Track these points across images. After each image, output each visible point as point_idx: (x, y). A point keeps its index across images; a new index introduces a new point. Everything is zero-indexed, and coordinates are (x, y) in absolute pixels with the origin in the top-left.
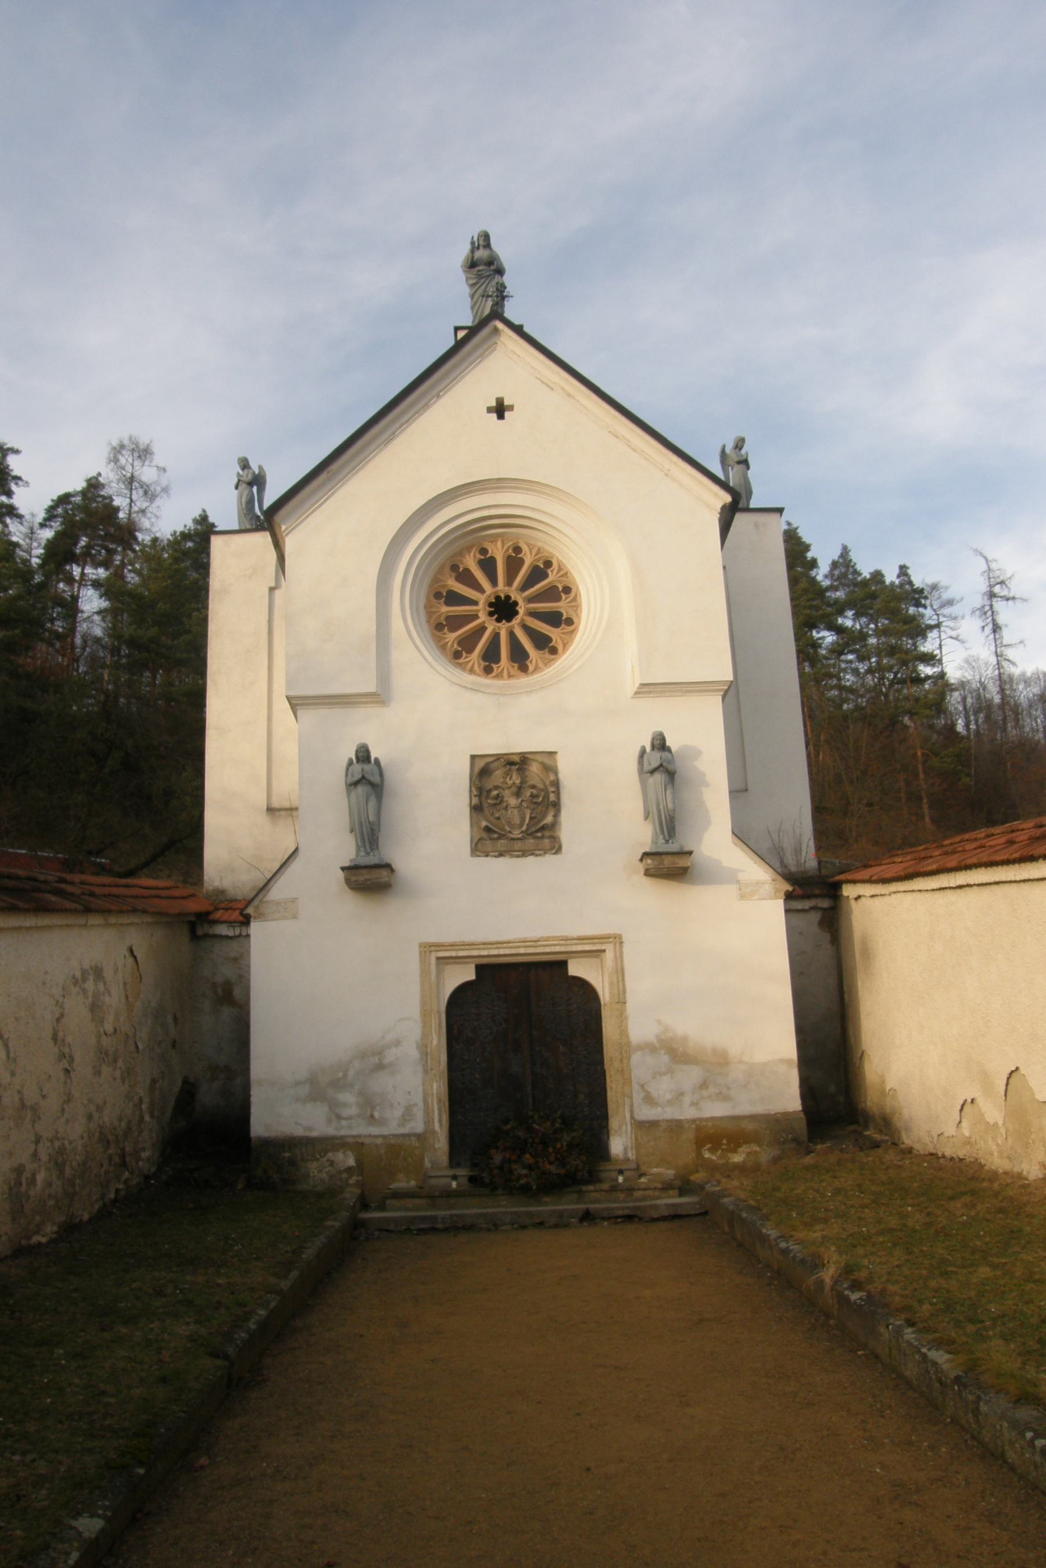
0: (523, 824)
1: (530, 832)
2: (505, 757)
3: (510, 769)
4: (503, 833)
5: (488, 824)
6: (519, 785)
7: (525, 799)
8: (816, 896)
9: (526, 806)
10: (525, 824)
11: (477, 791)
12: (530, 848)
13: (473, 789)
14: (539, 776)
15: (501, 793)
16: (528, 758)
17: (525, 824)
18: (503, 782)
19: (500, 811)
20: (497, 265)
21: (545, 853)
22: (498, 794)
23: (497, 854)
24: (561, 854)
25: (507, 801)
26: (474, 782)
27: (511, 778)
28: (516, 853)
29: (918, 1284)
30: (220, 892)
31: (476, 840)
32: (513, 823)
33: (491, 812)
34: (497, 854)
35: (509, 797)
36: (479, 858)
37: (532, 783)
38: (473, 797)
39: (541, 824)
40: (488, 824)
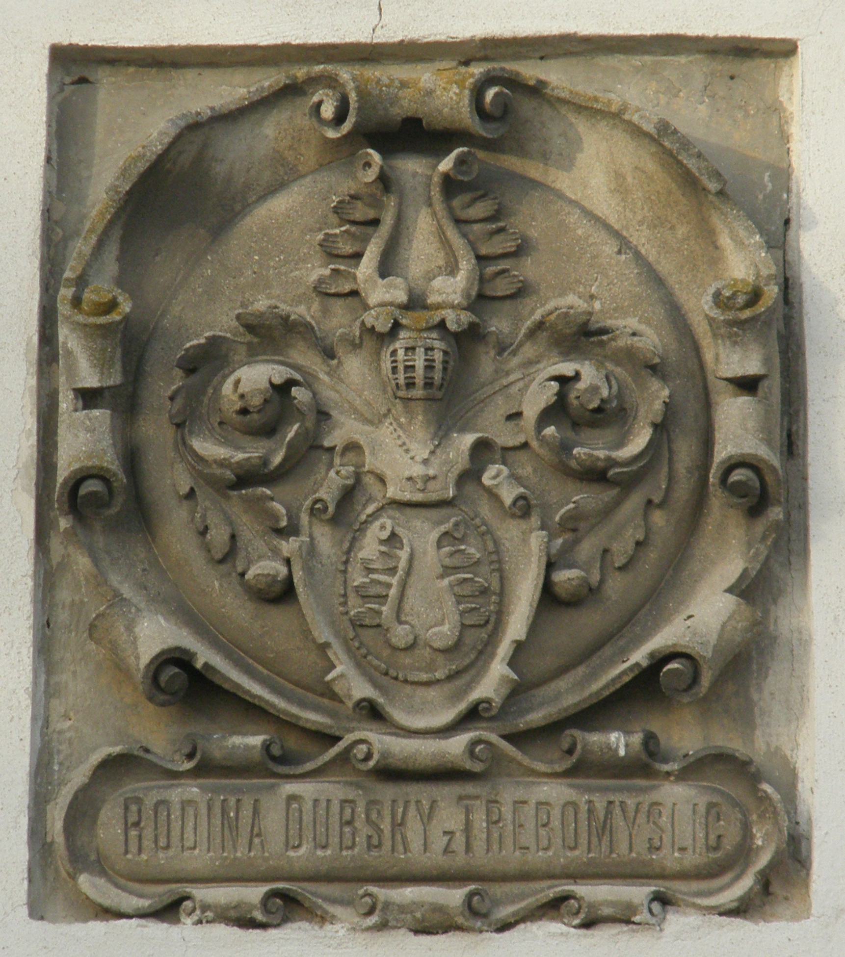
0: (486, 650)
1: (536, 717)
2: (345, 74)
3: (385, 181)
4: (313, 718)
5: (186, 639)
6: (455, 320)
7: (506, 437)
8: (445, 369)
9: (508, 495)
10: (504, 649)
11: (102, 364)
12: (538, 858)
13: (66, 336)
14: (624, 244)
15: (309, 381)
16: (537, 90)
17: (504, 649)
18: (321, 291)
19: (292, 530)
20: (204, 753)
21: (663, 900)
22: (283, 389)
23: (254, 893)
24: (804, 913)
25: (352, 447)
26: (81, 282)
27: (385, 268)
28: (409, 893)
29: (230, 281)
30: (575, 159)
31: (79, 776)
32: (400, 635)
33: (219, 535)
34: (254, 893)
35: (375, 421)
36: (98, 928)
37: (572, 301)
38: (66, 402)
39: (639, 656)
40: (186, 639)
